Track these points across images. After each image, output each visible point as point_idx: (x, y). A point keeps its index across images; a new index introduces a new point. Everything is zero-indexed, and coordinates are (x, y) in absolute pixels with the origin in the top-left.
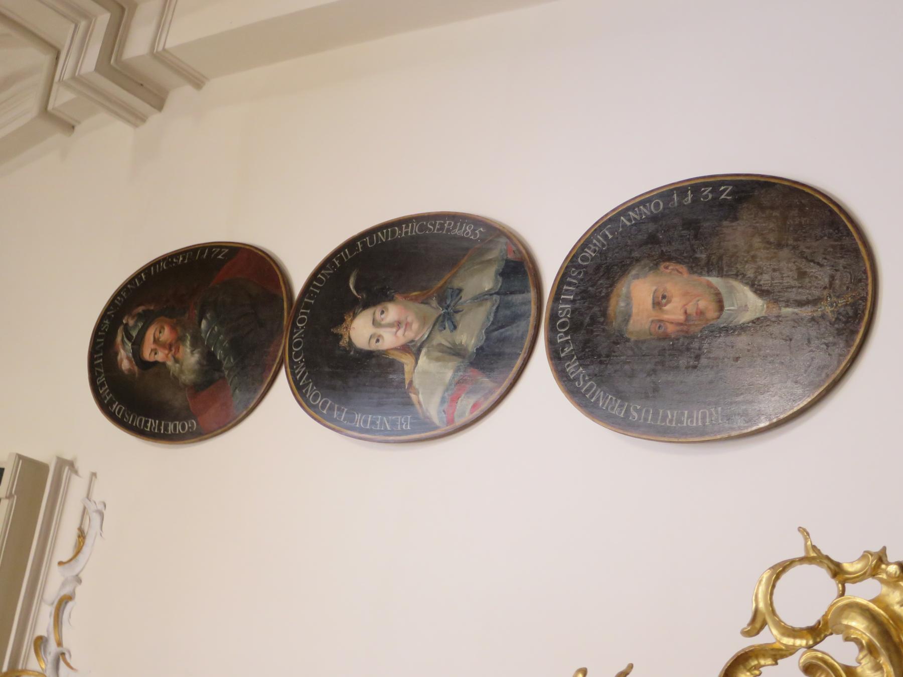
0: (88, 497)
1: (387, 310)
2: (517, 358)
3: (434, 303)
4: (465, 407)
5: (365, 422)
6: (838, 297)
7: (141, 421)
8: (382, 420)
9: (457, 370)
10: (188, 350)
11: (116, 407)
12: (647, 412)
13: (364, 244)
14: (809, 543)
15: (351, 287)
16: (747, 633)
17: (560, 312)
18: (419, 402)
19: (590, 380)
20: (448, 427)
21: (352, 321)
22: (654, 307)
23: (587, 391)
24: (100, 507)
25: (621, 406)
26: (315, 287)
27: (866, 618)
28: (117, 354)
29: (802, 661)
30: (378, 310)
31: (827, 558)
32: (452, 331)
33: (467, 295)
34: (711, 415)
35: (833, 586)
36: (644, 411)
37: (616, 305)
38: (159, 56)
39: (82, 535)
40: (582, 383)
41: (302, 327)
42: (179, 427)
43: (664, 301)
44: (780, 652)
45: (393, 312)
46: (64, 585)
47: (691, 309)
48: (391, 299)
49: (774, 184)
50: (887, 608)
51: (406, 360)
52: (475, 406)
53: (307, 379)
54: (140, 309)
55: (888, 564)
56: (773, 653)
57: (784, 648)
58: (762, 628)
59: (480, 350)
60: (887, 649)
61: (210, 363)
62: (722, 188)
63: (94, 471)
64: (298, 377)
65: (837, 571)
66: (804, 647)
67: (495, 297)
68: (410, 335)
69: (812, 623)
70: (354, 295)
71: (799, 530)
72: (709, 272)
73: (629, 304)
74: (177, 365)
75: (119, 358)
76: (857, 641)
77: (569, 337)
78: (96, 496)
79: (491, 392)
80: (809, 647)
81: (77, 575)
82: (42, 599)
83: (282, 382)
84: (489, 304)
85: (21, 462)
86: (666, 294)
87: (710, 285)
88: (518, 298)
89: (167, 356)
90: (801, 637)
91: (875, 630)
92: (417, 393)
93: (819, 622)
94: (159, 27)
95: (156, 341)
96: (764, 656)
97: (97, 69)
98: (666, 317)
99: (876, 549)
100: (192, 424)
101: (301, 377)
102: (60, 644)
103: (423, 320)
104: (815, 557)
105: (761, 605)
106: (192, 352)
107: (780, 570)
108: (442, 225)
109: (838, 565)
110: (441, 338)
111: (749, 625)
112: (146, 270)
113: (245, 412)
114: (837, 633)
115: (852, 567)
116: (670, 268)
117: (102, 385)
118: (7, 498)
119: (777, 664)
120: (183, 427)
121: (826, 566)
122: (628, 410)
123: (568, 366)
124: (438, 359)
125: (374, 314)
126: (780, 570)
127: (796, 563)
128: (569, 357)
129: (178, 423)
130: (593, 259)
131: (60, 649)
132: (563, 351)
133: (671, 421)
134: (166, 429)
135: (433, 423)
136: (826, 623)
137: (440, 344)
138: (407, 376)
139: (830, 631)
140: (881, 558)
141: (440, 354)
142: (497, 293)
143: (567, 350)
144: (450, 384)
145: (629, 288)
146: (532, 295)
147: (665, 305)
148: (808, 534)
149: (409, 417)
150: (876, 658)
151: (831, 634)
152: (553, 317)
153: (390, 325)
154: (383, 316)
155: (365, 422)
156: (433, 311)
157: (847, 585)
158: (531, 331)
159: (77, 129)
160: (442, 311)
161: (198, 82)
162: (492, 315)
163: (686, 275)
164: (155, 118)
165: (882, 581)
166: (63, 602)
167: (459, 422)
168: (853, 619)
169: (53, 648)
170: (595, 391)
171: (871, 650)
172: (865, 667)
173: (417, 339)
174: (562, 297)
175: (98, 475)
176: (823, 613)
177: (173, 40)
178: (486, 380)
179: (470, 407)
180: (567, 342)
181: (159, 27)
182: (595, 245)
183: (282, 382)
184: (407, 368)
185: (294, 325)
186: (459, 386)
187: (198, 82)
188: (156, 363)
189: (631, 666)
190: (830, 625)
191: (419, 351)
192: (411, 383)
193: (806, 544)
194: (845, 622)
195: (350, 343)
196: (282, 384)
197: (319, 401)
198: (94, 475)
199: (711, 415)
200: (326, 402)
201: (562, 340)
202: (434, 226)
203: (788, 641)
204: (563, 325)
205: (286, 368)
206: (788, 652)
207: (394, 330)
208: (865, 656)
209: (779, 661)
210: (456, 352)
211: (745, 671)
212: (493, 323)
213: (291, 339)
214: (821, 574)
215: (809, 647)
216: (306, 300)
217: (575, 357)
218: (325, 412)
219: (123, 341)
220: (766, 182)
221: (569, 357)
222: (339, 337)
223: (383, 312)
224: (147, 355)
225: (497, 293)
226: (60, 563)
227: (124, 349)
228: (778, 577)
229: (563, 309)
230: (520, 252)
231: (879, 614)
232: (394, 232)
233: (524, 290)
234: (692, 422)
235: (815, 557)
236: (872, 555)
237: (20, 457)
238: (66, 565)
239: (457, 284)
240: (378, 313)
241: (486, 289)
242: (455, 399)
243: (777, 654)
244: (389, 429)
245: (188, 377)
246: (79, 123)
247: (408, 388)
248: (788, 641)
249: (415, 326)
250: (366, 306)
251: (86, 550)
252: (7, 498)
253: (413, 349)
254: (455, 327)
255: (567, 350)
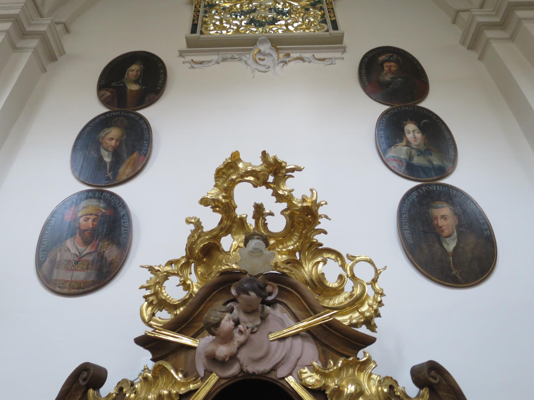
0: (336, 59)
1: (419, 133)
2: (413, 177)
3: (425, 148)
4: (393, 164)
5: (381, 135)
6: (460, 275)
7: (364, 68)
8: (383, 139)
9: (405, 159)
10: (390, 77)
11: (367, 59)
12: (406, 220)
13: (439, 122)
14: (382, 270)
15: (424, 121)
16: (347, 255)
17: (433, 186)
18: (391, 149)
19: (412, 200)
20: (386, 160)
21: (413, 123)
22: (441, 216)
23: (409, 200)
24: (334, 63)
25: (406, 211)
26: (421, 110)
27: (362, 292)
28: (384, 55)
29: (343, 274)
30: (418, 131)
31: (378, 277)
32: (417, 155)
33: (430, 157)
34: (410, 240)
35: (369, 280)
36: (406, 218)
37: (439, 204)
38: (488, 41)
39: (323, 60)
40: (411, 197)
41: (407, 109)
42: (365, 80)
43: (444, 219)
44: (344, 267)
45: (419, 135)
46: (307, 58)
47: (443, 228)
48: (423, 134)
49: (494, 249)
50: (366, 299)
51: (404, 143)
52: (394, 167)
53: (391, 114)
54: (399, 59)
55: (381, 297)
56: (343, 264)
57: (346, 268)
58: (351, 260)
59: (413, 165)
60: (353, 301)
61: (386, 85)
62: (488, 231)
63: (344, 58)
64: (390, 111)
65: (374, 281)
66: (347, 274)
67: (432, 166)
68: (413, 142)
69: (356, 275)
70: (422, 122)
71: (385, 266)
72: (457, 232)
73: (439, 208)
74: (384, 74)
75: (383, 56)
76: (353, 290)
77: (425, 191)
78: (337, 61)
79: (400, 171)
80: (348, 276)
81: (311, 61)
82: (301, 53)
83: (386, 108)
84: (429, 164)
85: (342, 35)
86: (447, 219)
87: (453, 233)
88: (433, 173)
89: (387, 70)
90: (350, 272)
91: (358, 296)
92: (394, 148)
93: (356, 278)
94: (499, 39)
95: (390, 66)
96: (341, 262)
97: (478, 23)
98: (439, 220)
99: (384, 293)
100: (367, 84)
101: (391, 112)
102: (289, 61)
103: (418, 145)
104: (377, 273)
105: (358, 258)
106: (390, 78)
107: (371, 262)
108: (452, 145)
109: (376, 281)
110: (414, 152)
111: (351, 255)
112: (413, 58)
113: (374, 98)
114: (354, 284)
115: (377, 286)
116: (456, 219)
117: (372, 53)
118: (330, 33)
119: (340, 266)
120: (365, 81)
121: (375, 277)
122: (405, 213)
123: (415, 192)
124: (407, 153)
125: (417, 130)
126: (371, 262)
127: (374, 267)
128: (418, 192)
129: (366, 79)
130: (453, 194)
131: (288, 62)
132: (420, 190)
133: (404, 227)
134: (363, 76)
135: (386, 156)
136: (356, 280)
137: (412, 152)
138: (399, 144)
139: (354, 282)
140: (382, 295)
141: (409, 153)
142: (433, 167)
143: (420, 191)
144: (400, 158)
145: (446, 207)
146: (435, 178)
147: (443, 219)
148: (385, 269)
149: (386, 148)
150: (349, 297)
151: (353, 282)
152: (430, 185)
153: (414, 136)
154: (417, 133)
155: (381, 135)
156: (422, 148)
157: (370, 285)
158: (423, 179)
159: (454, 25)
160: (423, 150)
161: (480, 58)
162: (426, 166)
163: (455, 224)
164: (464, 48)
165: (374, 296)
166: (302, 59)
167: (388, 163)
168: (360, 288)
169: (287, 60)
170: (409, 202)
171: (351, 295)
172: (345, 295)
173: (412, 145)
174: (438, 187)
175: (343, 60)
176: (360, 279)
177: (495, 45)
178: (404, 169)
179: (394, 165)
180: (423, 190)
181: (499, 39)
182: (458, 194)
183: (386, 108)
184: (402, 144)
185: (406, 106)
186: (399, 160)
187: (480, 58)
188: (383, 68)
189: (330, 219)
190: (357, 281)
191: (408, 146)
192: (397, 146)
193: (381, 269)
194: (359, 286)
195: (406, 125)
196: (386, 108)
197: (384, 119)
198: (343, 59)
199: (410, 240)
200: (384, 121)
201: (423, 189)
202: (451, 142)
203: (348, 269)
204: (428, 188)
205: (227, 382)
206: (345, 270)
207: (413, 137)
208: (348, 294)
209: (341, 267)
210: (411, 157)
211: (335, 257)
212: (423, 167)
213: (402, 106)
214: (372, 276)
215: (348, 276)
216: (416, 108)
217: (419, 194)
218: (381, 122)
219: (388, 56)
220: (494, 245)
221: (418, 192)
222: (406, 120)
223: (418, 132)
224: (385, 64)
225: (433, 167)
226: (314, 55)
227: (386, 57)
228: (368, 262)
229: (434, 187)
230: (449, 171)
231: (363, 296)
232: (446, 130)
233: (436, 175)
234: (406, 234)
235: (377, 273)
236: (382, 291)
237: (343, 34)
238: (313, 57)
239: (433, 153)
240: (417, 131)
241: (434, 163)
242: (395, 160)
243: (343, 266)
244: (381, 142)
245: (381, 79)
246: (456, 25)
247: (395, 145)
248: (348, 269)
249: (416, 143)
250: (419, 127)
251: (320, 62)
252: (330, 33)
253: (408, 144)
254: (419, 156)
255: (420, 191)
